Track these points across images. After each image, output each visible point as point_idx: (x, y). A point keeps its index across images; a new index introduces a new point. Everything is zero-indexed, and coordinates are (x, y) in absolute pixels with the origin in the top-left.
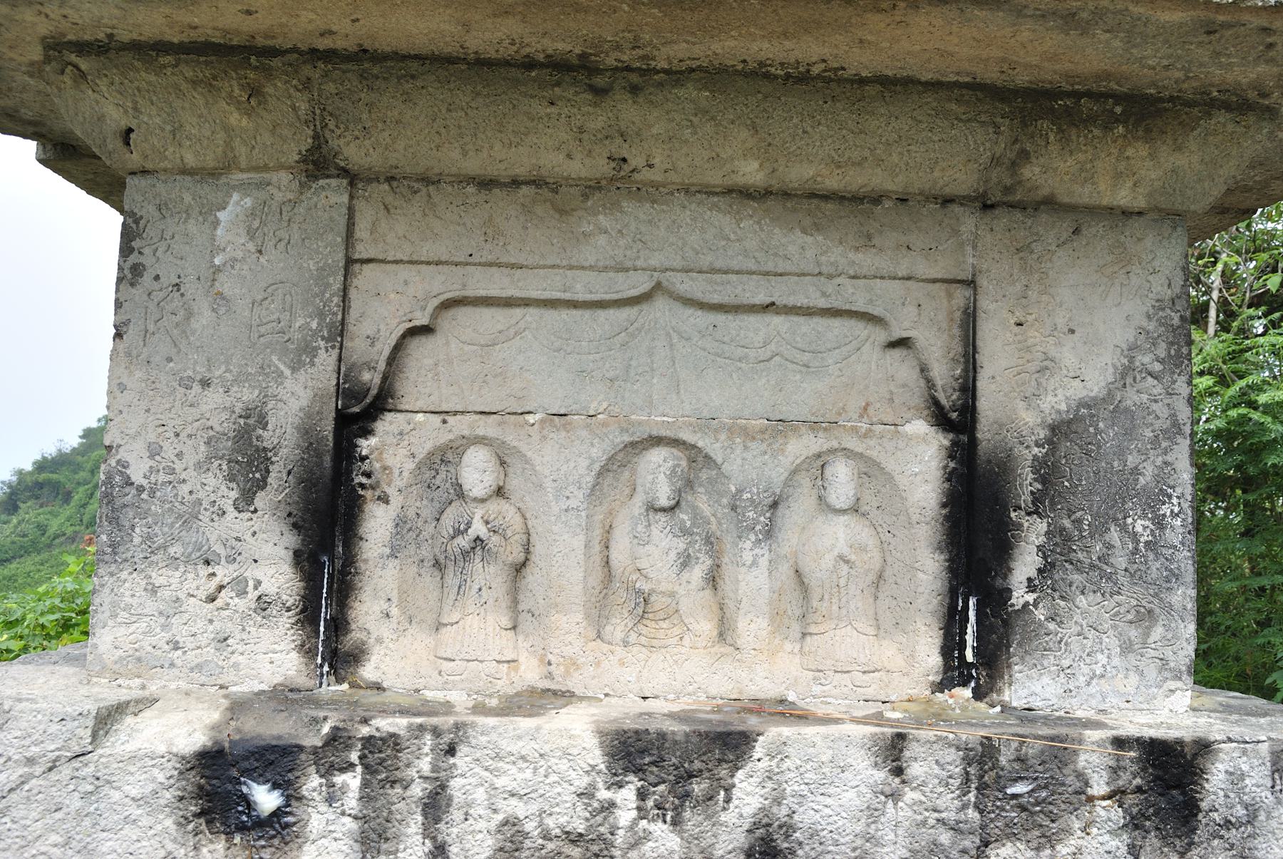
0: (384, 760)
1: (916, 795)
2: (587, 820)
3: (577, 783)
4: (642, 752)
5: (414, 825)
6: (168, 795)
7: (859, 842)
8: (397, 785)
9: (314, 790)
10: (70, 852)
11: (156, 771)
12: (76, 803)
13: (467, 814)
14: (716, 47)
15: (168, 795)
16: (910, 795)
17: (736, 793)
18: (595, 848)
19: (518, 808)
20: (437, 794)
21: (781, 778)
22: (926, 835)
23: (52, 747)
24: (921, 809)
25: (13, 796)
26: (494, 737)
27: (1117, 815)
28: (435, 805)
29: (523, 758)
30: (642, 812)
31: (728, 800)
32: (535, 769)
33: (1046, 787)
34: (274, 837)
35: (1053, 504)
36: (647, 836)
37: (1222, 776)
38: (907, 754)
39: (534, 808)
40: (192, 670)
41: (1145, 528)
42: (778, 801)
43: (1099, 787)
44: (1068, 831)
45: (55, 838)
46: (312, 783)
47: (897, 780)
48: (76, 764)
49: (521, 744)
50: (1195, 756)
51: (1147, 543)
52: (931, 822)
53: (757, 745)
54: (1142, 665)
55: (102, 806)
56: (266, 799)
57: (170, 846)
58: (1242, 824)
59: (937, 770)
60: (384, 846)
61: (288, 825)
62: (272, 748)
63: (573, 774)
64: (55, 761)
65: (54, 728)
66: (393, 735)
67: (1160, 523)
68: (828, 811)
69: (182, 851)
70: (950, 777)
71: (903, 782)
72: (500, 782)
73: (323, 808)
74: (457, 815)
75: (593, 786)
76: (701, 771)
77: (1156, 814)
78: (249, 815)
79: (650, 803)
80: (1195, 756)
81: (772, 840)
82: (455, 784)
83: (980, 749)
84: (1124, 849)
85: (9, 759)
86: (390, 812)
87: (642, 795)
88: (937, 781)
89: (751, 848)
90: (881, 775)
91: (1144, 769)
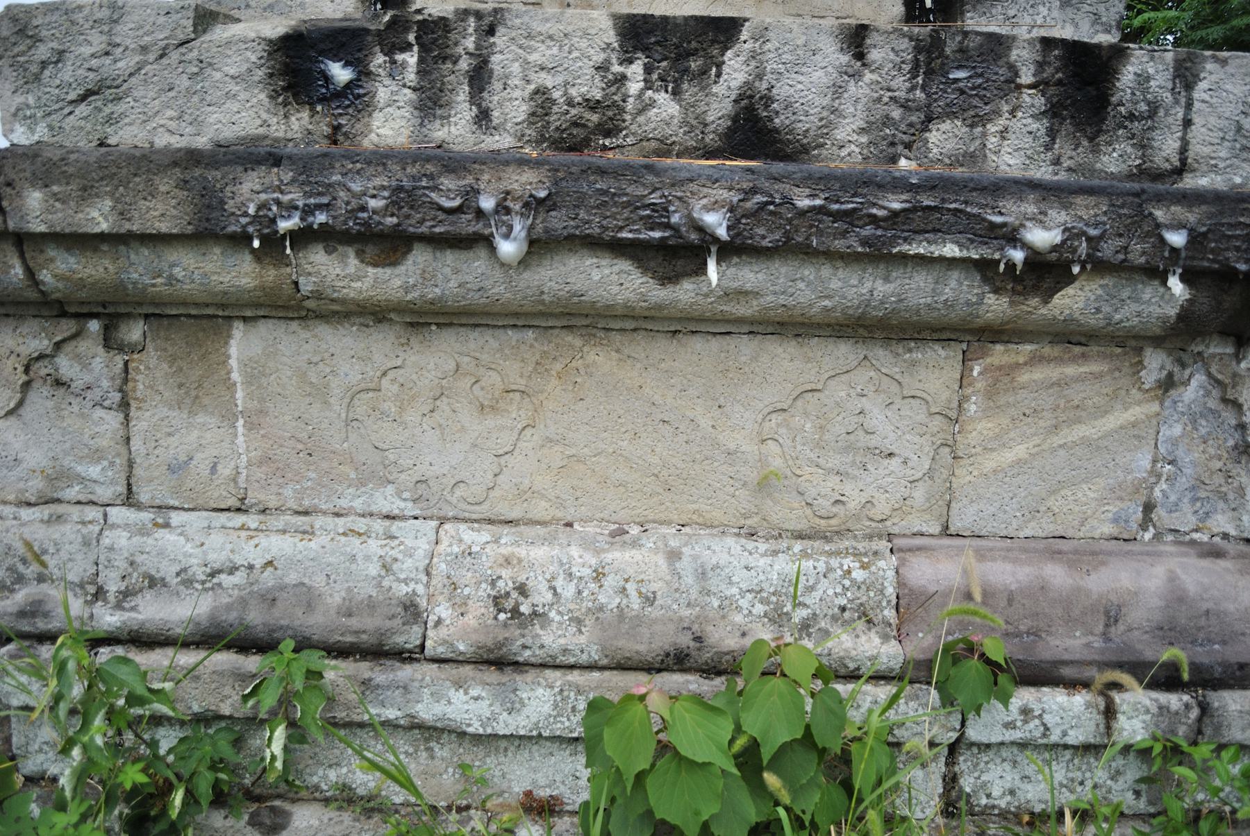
0: (436, 40)
1: (875, 77)
2: (603, 89)
3: (594, 58)
4: (650, 32)
5: (462, 95)
6: (260, 73)
7: (825, 114)
8: (448, 62)
9: (380, 66)
10: (184, 124)
11: (249, 54)
12: (184, 82)
13: (505, 84)
14: (882, 288)
15: (260, 73)
16: (869, 76)
17: (725, 69)
18: (610, 113)
19: (548, 80)
20: (481, 68)
21: (764, 58)
22: (880, 110)
23: (162, 37)
24: (877, 88)
25: (133, 80)
26: (526, 19)
27: (1040, 102)
28: (480, 77)
29: (551, 37)
30: (648, 85)
31: (719, 75)
32: (561, 46)
33: (981, 75)
34: (349, 106)
36: (652, 103)
37: (1131, 77)
38: (868, 41)
39: (560, 79)
40: (265, 9)
42: (760, 77)
43: (1026, 77)
44: (998, 113)
45: (170, 113)
46: (378, 60)
47: (859, 64)
48: (183, 50)
49: (548, 25)
50: (1110, 58)
52: (886, 99)
53: (744, 29)
54: (1077, 18)
55: (207, 84)
56: (340, 73)
57: (265, 116)
58: (1143, 118)
59: (892, 56)
60: (439, 112)
61: (359, 96)
62: (343, 31)
63: (592, 52)
64: (164, 49)
65: (162, 19)
66: (443, 18)
68: (800, 86)
69: (275, 120)
70: (903, 62)
71: (864, 65)
72: (533, 58)
73: (387, 81)
74: (497, 85)
75: (608, 61)
76: (697, 50)
77: (1073, 104)
78: (327, 88)
79: (655, 76)
80: (1110, 58)
81: (754, 110)
82: (496, 59)
83: (929, 40)
84: (1043, 131)
85: (127, 48)
86: (443, 84)
87: (648, 70)
88: (891, 65)
89: (737, 115)
90: (845, 59)
91: (1066, 66)
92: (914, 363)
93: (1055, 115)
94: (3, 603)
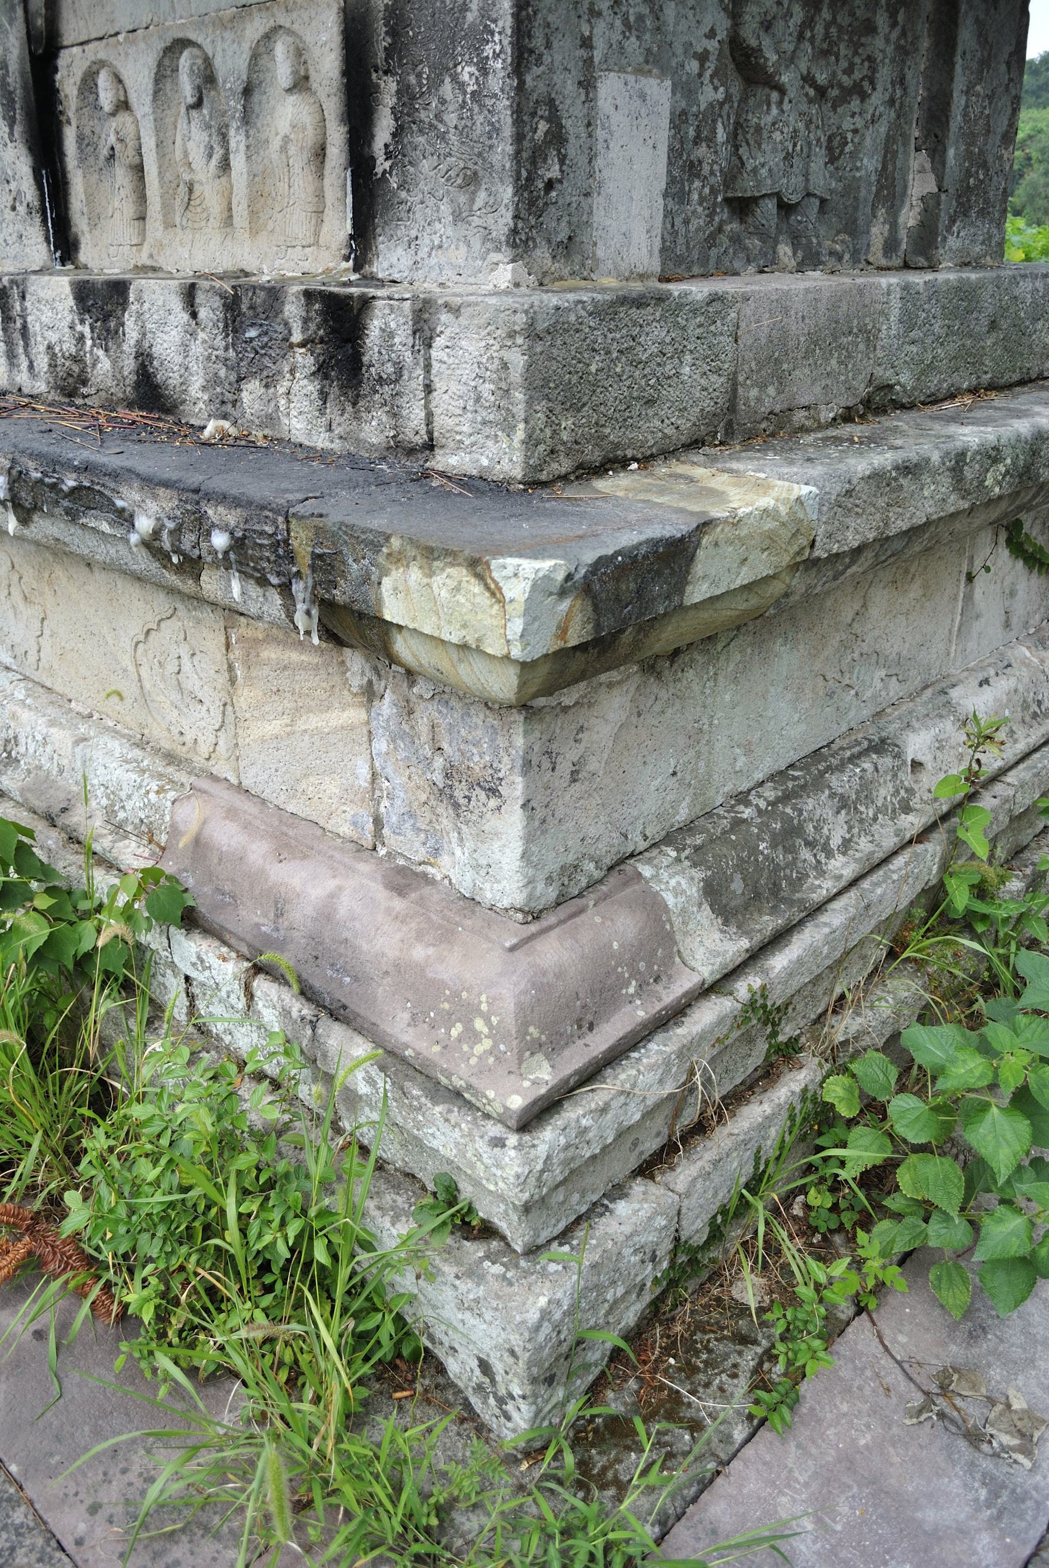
35: (400, 60)
37: (377, 332)
41: (471, 75)
51: (473, 93)
67: (484, 70)
91: (325, 321)
92: (198, 622)
93: (326, 376)
94: (1042, 730)
